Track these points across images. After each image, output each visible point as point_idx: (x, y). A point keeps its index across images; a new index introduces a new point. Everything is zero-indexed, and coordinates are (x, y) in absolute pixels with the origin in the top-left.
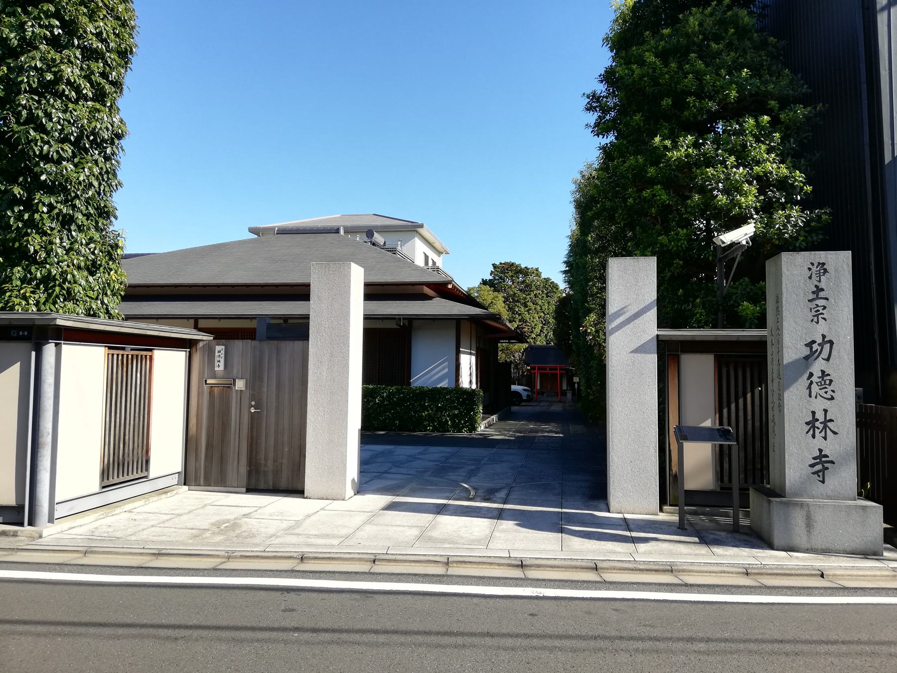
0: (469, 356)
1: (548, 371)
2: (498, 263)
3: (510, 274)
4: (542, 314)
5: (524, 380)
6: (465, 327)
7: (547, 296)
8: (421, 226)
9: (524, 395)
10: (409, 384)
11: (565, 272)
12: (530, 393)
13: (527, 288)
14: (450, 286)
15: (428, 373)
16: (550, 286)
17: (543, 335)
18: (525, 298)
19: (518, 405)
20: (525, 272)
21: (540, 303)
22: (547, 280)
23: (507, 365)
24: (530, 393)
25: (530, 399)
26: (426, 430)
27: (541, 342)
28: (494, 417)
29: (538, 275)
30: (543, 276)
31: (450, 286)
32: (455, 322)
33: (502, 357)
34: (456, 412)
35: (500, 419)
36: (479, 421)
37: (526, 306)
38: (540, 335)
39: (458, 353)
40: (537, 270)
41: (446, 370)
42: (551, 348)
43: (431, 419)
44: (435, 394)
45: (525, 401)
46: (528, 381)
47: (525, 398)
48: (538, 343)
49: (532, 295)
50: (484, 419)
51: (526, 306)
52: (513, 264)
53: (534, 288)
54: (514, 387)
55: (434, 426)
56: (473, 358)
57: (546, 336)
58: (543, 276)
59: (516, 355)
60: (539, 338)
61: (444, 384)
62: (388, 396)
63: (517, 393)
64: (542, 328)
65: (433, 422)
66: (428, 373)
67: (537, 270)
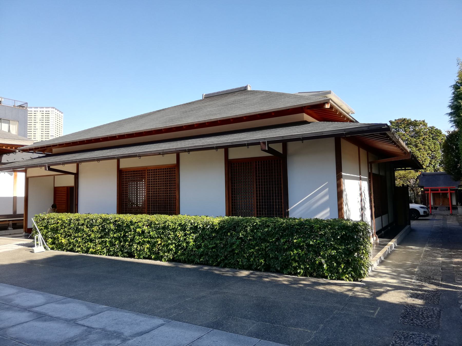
0: (357, 182)
1: (440, 191)
2: (393, 120)
3: (403, 126)
4: (430, 152)
5: (419, 199)
6: (345, 144)
7: (433, 139)
8: (329, 93)
9: (421, 211)
10: (287, 214)
11: (450, 114)
12: (426, 210)
13: (417, 134)
14: (327, 106)
15: (308, 199)
16: (434, 133)
17: (432, 166)
18: (416, 141)
19: (417, 219)
20: (415, 124)
21: (428, 144)
22: (432, 128)
23: (405, 189)
24: (426, 210)
25: (426, 214)
26: (296, 274)
27: (430, 170)
28: (392, 243)
29: (425, 125)
30: (429, 125)
31: (327, 106)
32: (333, 139)
33: (399, 183)
34: (334, 252)
35: (400, 243)
36: (371, 250)
37: (416, 146)
38: (429, 166)
39: (339, 177)
40: (424, 121)
41: (327, 198)
42: (441, 174)
43: (301, 260)
44: (308, 228)
45: (422, 216)
46: (424, 200)
47: (422, 213)
48: (428, 172)
49: (421, 138)
50: (380, 246)
51: (416, 146)
52: (405, 119)
53: (422, 134)
54: (412, 206)
55: (306, 269)
56: (365, 185)
57: (434, 167)
58: (429, 125)
59: (412, 181)
60: (429, 168)
61: (324, 215)
62: (252, 231)
63: (415, 210)
64: (431, 161)
65: (304, 263)
66: (308, 199)
67: (424, 121)
